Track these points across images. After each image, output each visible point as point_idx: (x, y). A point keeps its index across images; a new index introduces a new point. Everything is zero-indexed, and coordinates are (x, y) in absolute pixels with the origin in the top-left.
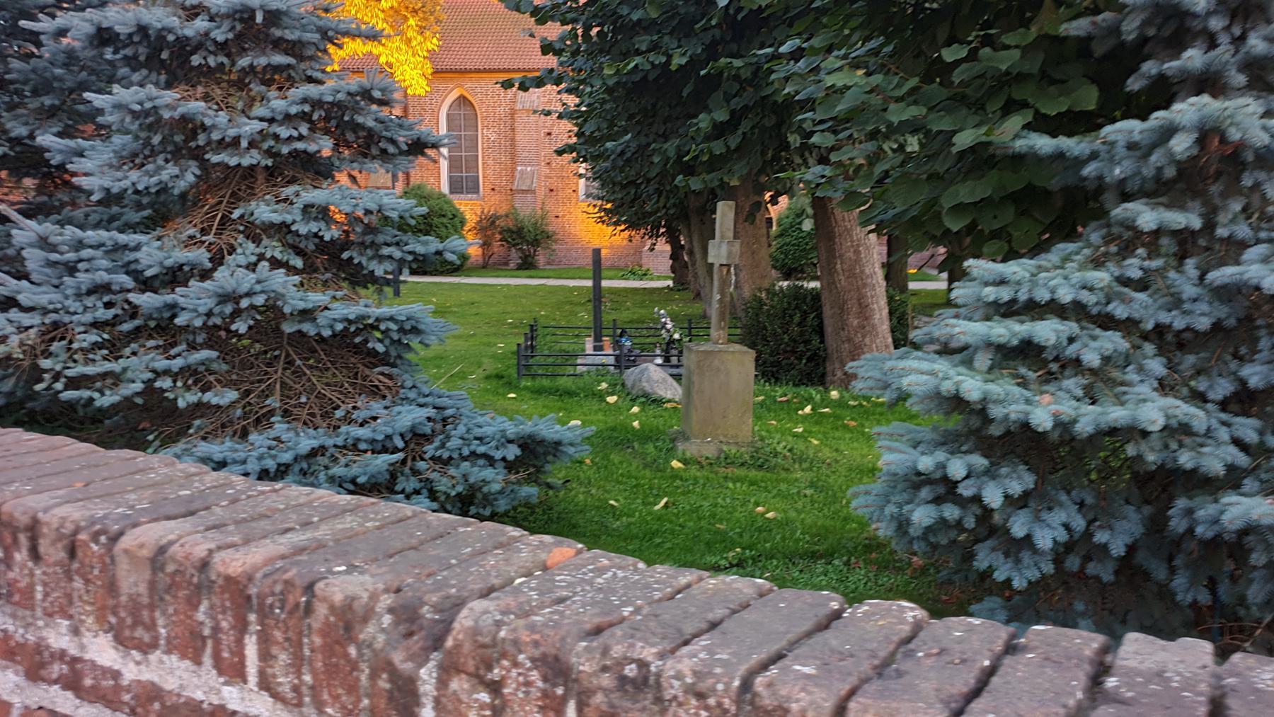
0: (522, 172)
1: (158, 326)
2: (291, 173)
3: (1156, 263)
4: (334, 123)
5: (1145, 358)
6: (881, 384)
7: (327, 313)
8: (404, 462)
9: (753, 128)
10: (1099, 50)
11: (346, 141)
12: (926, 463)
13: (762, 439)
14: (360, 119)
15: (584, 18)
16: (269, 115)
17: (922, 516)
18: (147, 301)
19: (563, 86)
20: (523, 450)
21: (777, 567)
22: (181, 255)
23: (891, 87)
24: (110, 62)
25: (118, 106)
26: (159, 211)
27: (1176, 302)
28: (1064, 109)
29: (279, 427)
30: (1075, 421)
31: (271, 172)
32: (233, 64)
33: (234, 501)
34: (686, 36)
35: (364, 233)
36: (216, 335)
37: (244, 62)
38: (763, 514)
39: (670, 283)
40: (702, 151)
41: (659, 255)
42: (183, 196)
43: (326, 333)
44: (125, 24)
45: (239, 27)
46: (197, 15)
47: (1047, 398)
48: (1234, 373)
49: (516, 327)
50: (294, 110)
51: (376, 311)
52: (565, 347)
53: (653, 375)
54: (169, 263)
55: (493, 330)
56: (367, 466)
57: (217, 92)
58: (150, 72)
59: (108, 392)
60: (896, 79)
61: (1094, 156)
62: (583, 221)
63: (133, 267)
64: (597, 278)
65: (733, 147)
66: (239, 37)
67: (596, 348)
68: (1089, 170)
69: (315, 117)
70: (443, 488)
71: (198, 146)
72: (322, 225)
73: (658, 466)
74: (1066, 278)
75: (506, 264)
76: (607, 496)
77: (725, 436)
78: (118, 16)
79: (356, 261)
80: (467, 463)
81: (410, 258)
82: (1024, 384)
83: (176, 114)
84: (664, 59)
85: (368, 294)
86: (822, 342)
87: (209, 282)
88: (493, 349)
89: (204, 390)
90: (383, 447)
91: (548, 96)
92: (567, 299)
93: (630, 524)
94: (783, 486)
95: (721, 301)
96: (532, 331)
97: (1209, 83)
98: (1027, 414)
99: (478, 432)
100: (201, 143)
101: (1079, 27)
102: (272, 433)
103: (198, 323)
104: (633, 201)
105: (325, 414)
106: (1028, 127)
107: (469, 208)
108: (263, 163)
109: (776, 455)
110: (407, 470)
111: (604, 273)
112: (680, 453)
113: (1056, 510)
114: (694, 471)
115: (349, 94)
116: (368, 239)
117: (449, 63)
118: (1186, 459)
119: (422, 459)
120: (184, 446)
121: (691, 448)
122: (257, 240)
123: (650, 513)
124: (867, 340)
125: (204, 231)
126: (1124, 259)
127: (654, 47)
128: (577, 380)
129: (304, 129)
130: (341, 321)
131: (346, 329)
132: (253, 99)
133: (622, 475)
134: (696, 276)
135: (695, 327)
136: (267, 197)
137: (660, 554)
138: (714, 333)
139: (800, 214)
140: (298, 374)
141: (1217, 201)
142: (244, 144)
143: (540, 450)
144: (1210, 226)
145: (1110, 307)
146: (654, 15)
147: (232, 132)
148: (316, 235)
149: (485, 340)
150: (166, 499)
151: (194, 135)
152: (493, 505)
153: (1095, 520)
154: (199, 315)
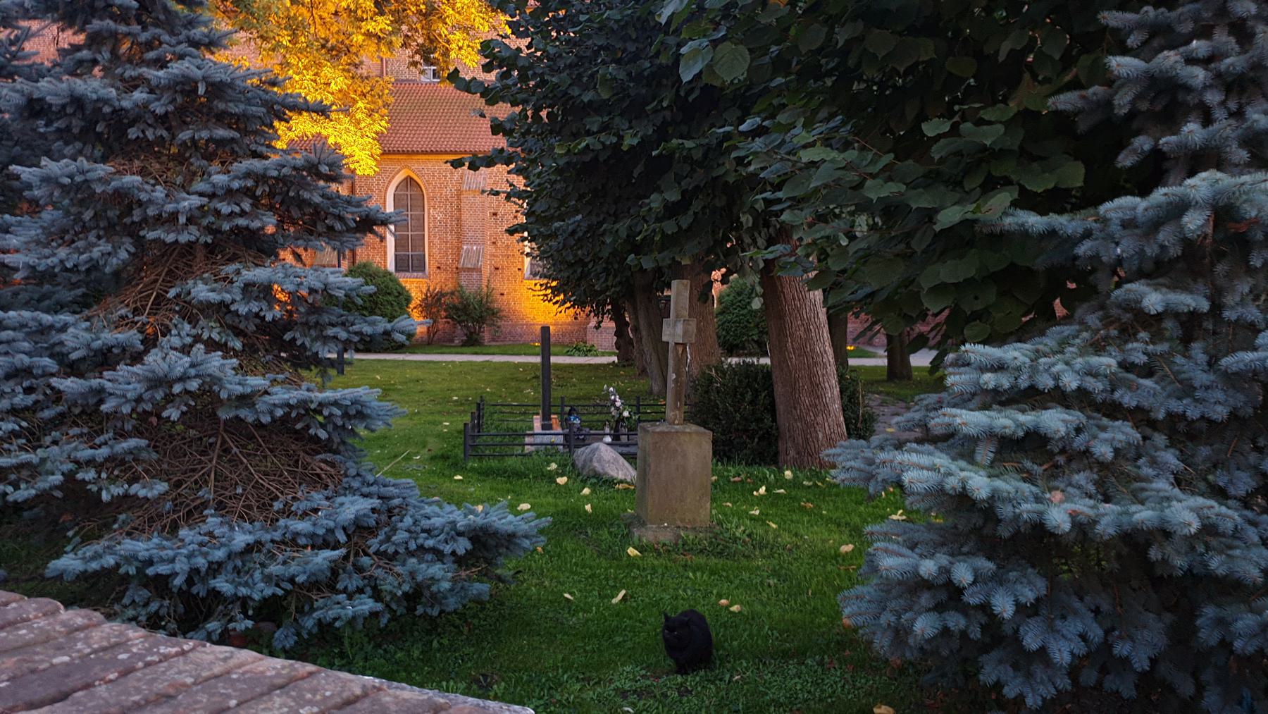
0: (468, 251)
1: (83, 412)
2: (232, 251)
3: (1161, 348)
4: (278, 198)
5: (1157, 449)
6: (863, 475)
7: (267, 398)
8: (346, 558)
9: (704, 208)
10: (1083, 126)
11: (290, 217)
12: (928, 567)
13: (720, 523)
14: (306, 195)
15: (534, 98)
16: (188, 180)
17: (924, 626)
18: (69, 384)
19: (512, 166)
20: (473, 544)
21: (747, 669)
22: (110, 337)
23: (864, 163)
24: (42, 135)
25: (47, 180)
26: (91, 291)
27: (1187, 389)
28: (1051, 186)
29: (213, 521)
30: (1095, 522)
31: (211, 249)
32: (173, 137)
33: (127, 672)
34: (636, 118)
35: (309, 313)
36: (146, 422)
37: (185, 135)
38: (727, 607)
39: (615, 359)
40: (654, 230)
41: (604, 334)
42: (117, 274)
43: (266, 419)
44: (56, 95)
45: (179, 100)
46: (136, 87)
47: (1058, 495)
48: (1256, 467)
49: (462, 404)
50: (236, 185)
51: (319, 396)
52: (512, 425)
53: (606, 457)
54: (97, 344)
55: (438, 408)
56: (307, 563)
57: (155, 166)
58: (85, 145)
59: (23, 486)
60: (870, 156)
61: (1088, 234)
62: (534, 304)
63: (57, 349)
64: (546, 354)
65: (684, 226)
66: (181, 111)
67: (544, 427)
68: (1084, 249)
69: (258, 192)
70: (388, 588)
71: (133, 223)
72: (264, 305)
73: (616, 555)
74: (1067, 363)
75: (452, 341)
76: (560, 587)
77: (682, 520)
78: (52, 87)
79: (299, 343)
80: (414, 560)
81: (356, 339)
82: (1030, 479)
83: (109, 189)
84: (615, 140)
85: (311, 376)
86: (774, 420)
87: (139, 366)
88: (439, 428)
89: (134, 480)
90: (323, 542)
91: (499, 176)
92: (513, 376)
93: (587, 620)
94: (745, 575)
95: (676, 381)
96: (479, 408)
97: (1198, 160)
98: (1041, 513)
99: (425, 523)
100: (136, 219)
101: (1066, 101)
102: (205, 528)
103: (126, 409)
104: (579, 279)
105: (261, 507)
106: (1015, 204)
107: (415, 286)
108: (202, 240)
109: (735, 540)
110: (349, 567)
111: (553, 349)
112: (636, 539)
113: (1070, 618)
114: (651, 560)
115: (295, 168)
116: (312, 319)
117: (396, 144)
118: (1217, 564)
119: (366, 554)
120: (106, 544)
121: (648, 535)
122: (193, 321)
123: (607, 608)
124: (819, 419)
125: (136, 311)
126: (1126, 342)
127: (605, 128)
128: (525, 460)
129: (246, 206)
130: (281, 406)
131: (287, 415)
132: (194, 174)
133: (576, 564)
134: (642, 353)
135: (646, 407)
136: (206, 275)
137: (620, 655)
138: (670, 414)
139: (751, 294)
140: (234, 462)
141: (1221, 282)
142: (182, 220)
143: (492, 542)
144: (1217, 308)
145: (1117, 395)
146: (605, 96)
147: (169, 207)
148: (257, 315)
149: (430, 418)
150: (33, 671)
151: (130, 209)
152: (441, 604)
153: (1113, 629)
154: (128, 401)
